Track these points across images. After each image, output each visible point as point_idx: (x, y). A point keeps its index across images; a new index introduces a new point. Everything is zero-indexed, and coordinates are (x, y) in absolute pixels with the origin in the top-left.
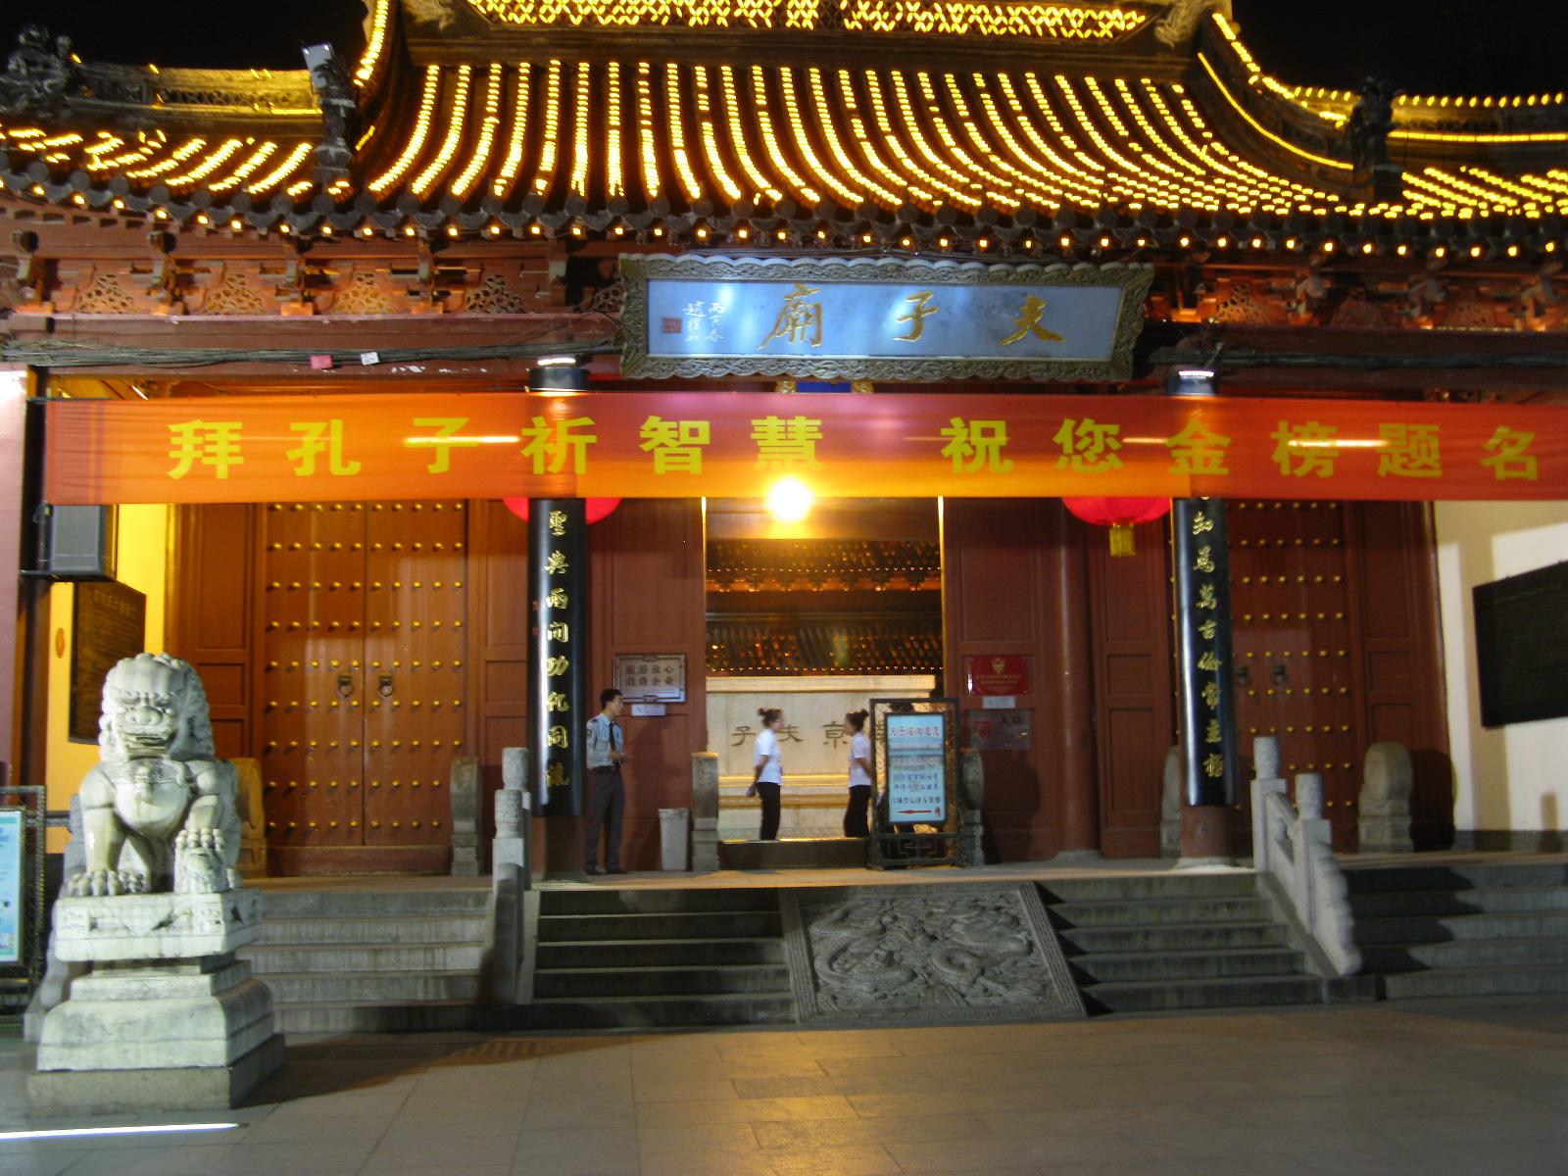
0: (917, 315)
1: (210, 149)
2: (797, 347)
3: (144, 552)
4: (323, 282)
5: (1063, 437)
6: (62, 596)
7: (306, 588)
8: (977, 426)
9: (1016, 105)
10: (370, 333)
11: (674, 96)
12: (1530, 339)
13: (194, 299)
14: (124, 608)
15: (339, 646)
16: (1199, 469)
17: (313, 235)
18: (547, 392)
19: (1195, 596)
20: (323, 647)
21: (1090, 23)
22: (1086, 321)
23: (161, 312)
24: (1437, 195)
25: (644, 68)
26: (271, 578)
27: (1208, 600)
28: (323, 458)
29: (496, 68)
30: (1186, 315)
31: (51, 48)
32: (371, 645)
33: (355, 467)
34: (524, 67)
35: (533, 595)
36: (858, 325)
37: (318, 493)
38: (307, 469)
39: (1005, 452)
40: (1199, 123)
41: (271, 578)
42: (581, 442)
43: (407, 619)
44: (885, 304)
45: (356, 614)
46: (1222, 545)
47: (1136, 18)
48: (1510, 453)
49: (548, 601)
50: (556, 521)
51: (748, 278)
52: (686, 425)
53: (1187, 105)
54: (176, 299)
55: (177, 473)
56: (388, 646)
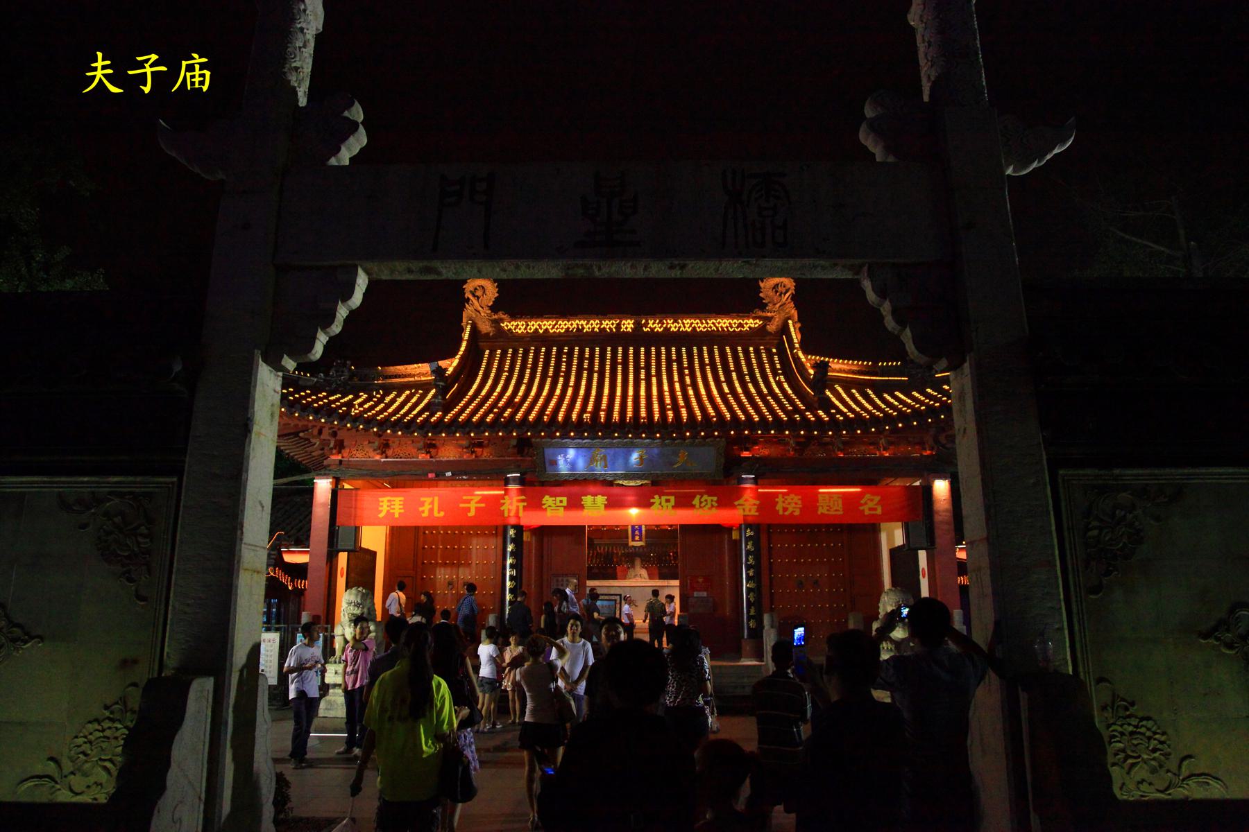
0: (641, 457)
1: (399, 396)
2: (599, 469)
3: (374, 539)
4: (434, 446)
5: (696, 502)
6: (343, 558)
7: (437, 548)
8: (664, 498)
9: (707, 361)
10: (450, 465)
11: (575, 361)
12: (883, 458)
13: (390, 452)
14: (368, 557)
15: (449, 570)
16: (747, 513)
17: (428, 431)
18: (510, 487)
19: (747, 560)
20: (442, 570)
21: (740, 325)
22: (707, 458)
23: (377, 458)
24: (844, 403)
25: (566, 349)
26: (424, 544)
27: (751, 561)
28: (431, 510)
29: (510, 351)
30: (746, 454)
31: (344, 365)
32: (461, 570)
33: (442, 514)
34: (521, 350)
35: (505, 559)
36: (620, 461)
37: (429, 523)
38: (426, 514)
39: (673, 507)
40: (778, 366)
41: (424, 544)
42: (521, 505)
43: (475, 561)
44: (628, 455)
45: (456, 558)
46: (755, 540)
47: (759, 322)
48: (871, 505)
49: (509, 561)
50: (511, 532)
51: (578, 447)
52: (558, 499)
53: (776, 358)
54: (383, 453)
55: (381, 515)
56: (467, 571)
